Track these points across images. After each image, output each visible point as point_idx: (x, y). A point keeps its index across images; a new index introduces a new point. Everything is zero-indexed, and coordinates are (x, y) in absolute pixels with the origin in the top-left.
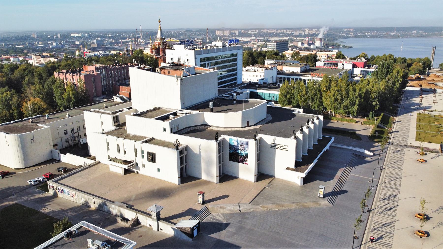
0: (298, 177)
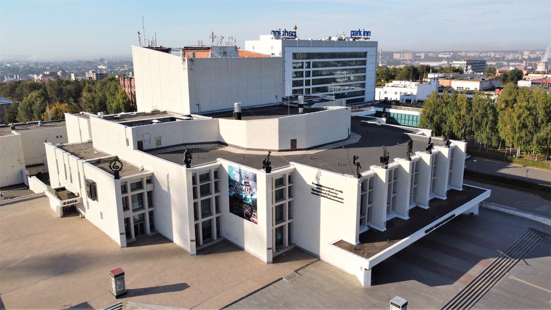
0: (361, 268)
